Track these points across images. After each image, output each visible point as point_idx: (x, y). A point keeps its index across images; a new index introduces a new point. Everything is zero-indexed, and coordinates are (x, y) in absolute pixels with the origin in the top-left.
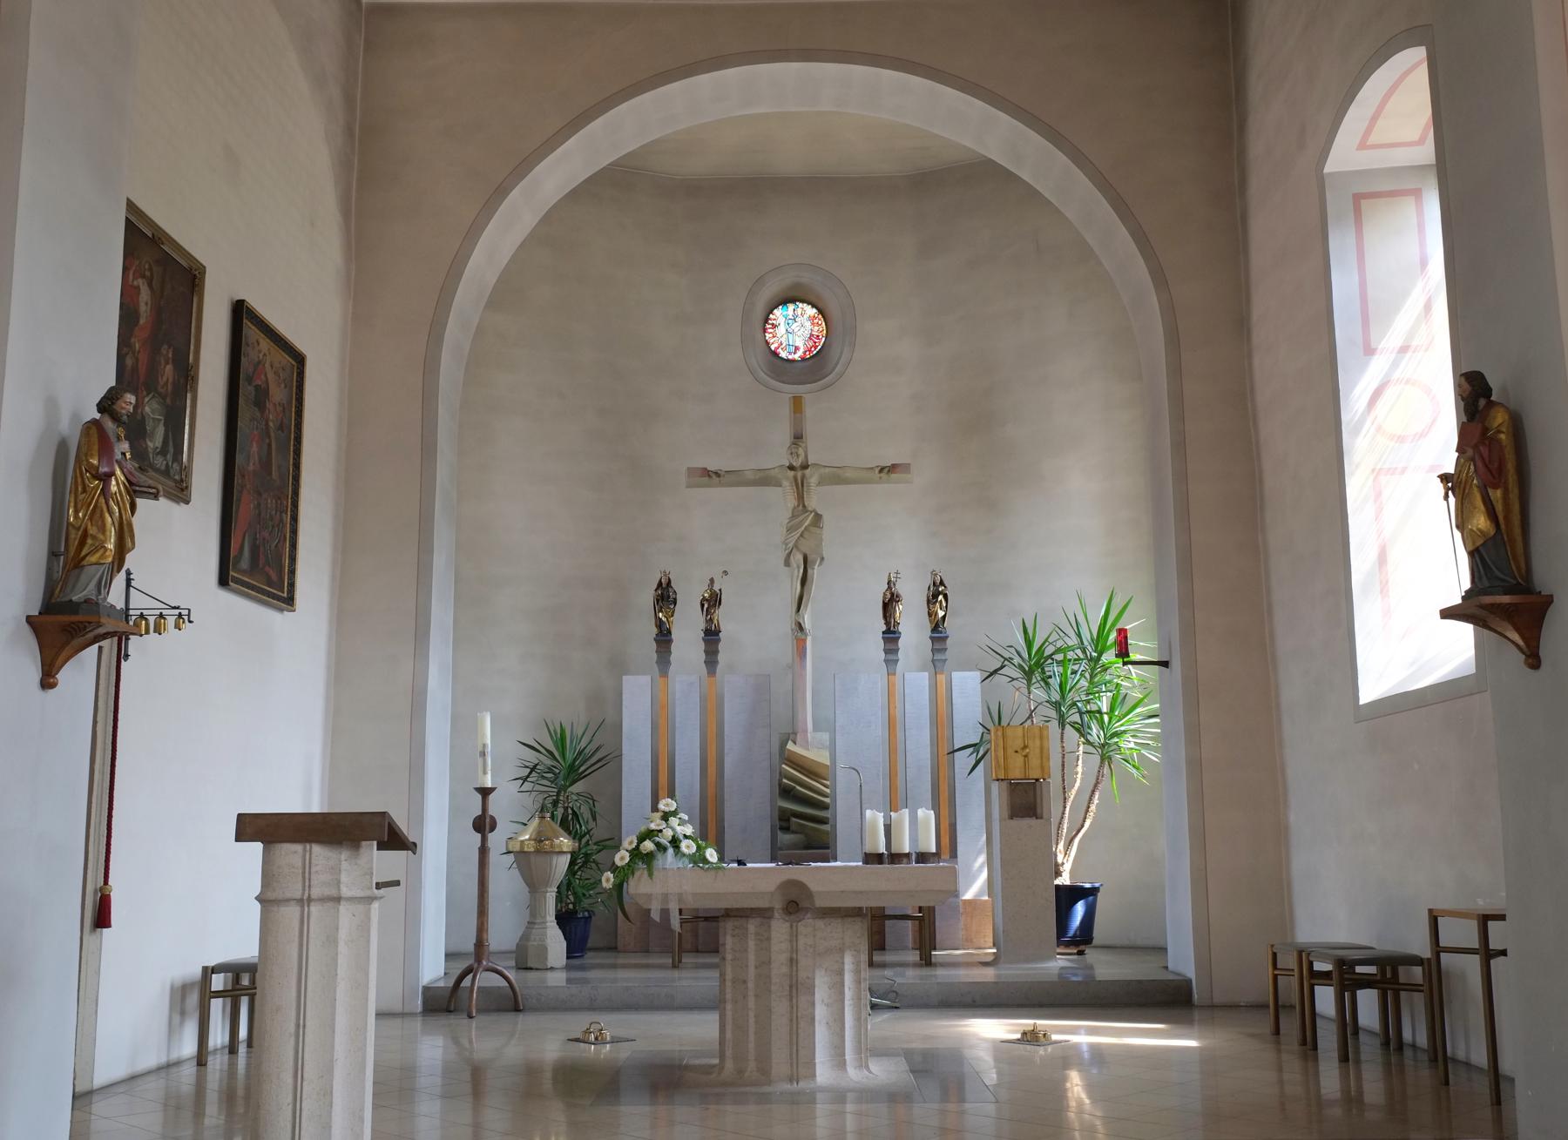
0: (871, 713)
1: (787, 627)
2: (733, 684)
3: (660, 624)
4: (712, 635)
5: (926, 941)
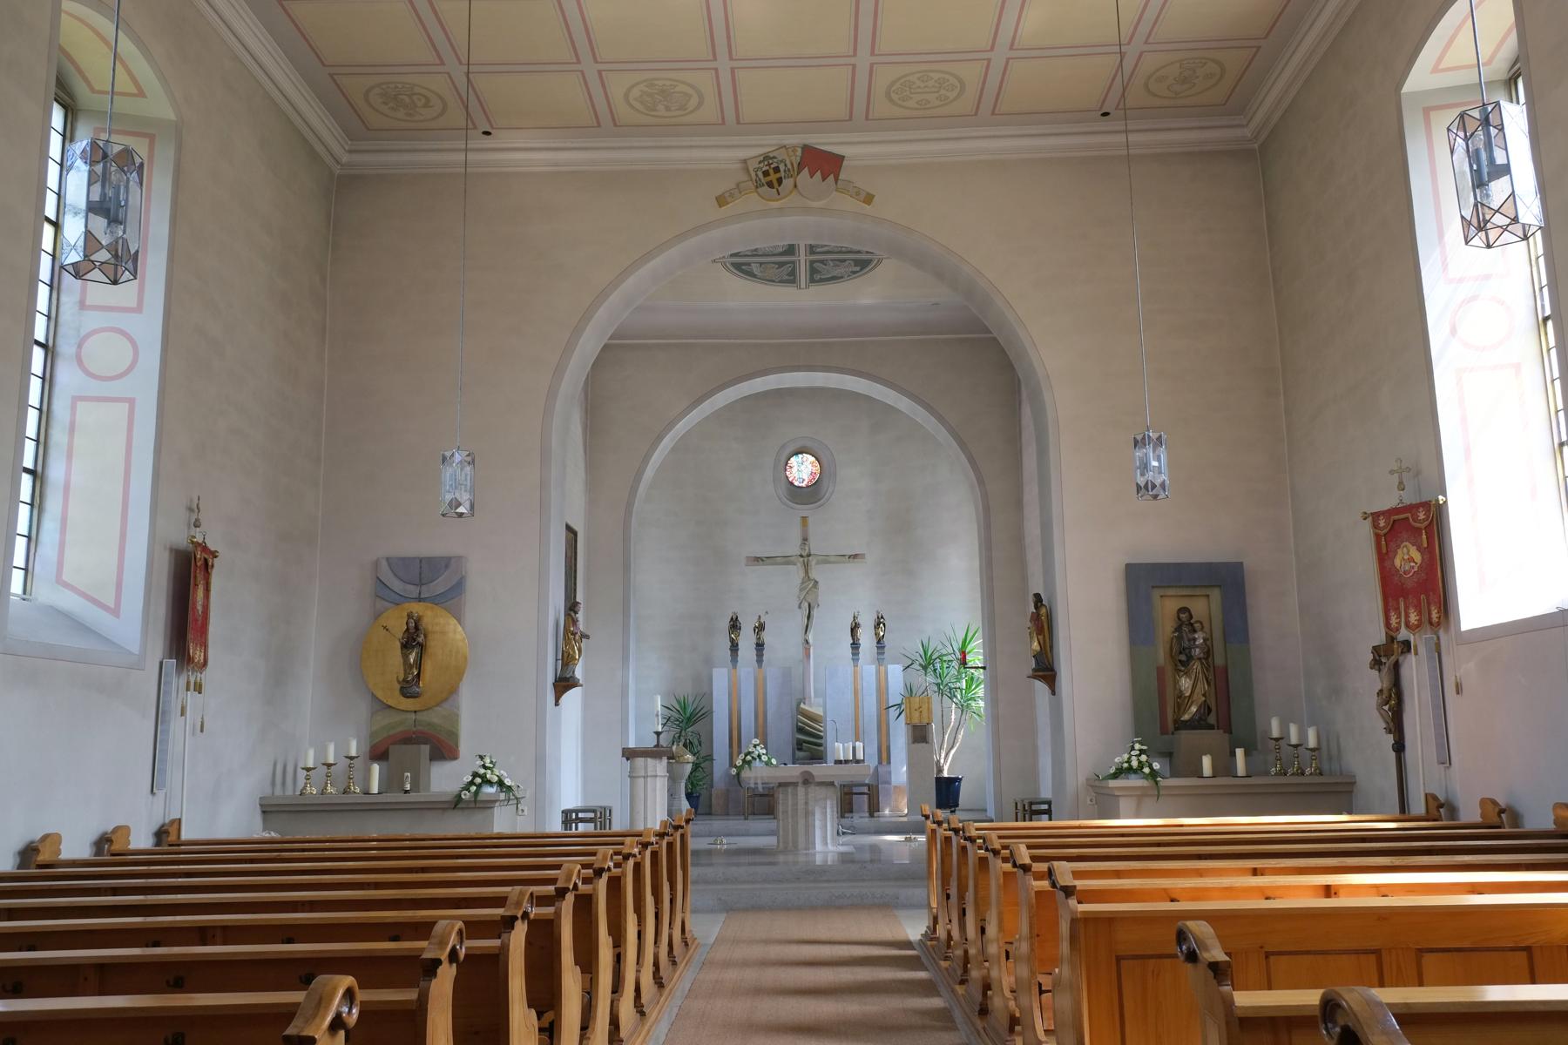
0: (845, 686)
1: (800, 639)
2: (772, 672)
3: (732, 640)
4: (760, 646)
5: (874, 809)
